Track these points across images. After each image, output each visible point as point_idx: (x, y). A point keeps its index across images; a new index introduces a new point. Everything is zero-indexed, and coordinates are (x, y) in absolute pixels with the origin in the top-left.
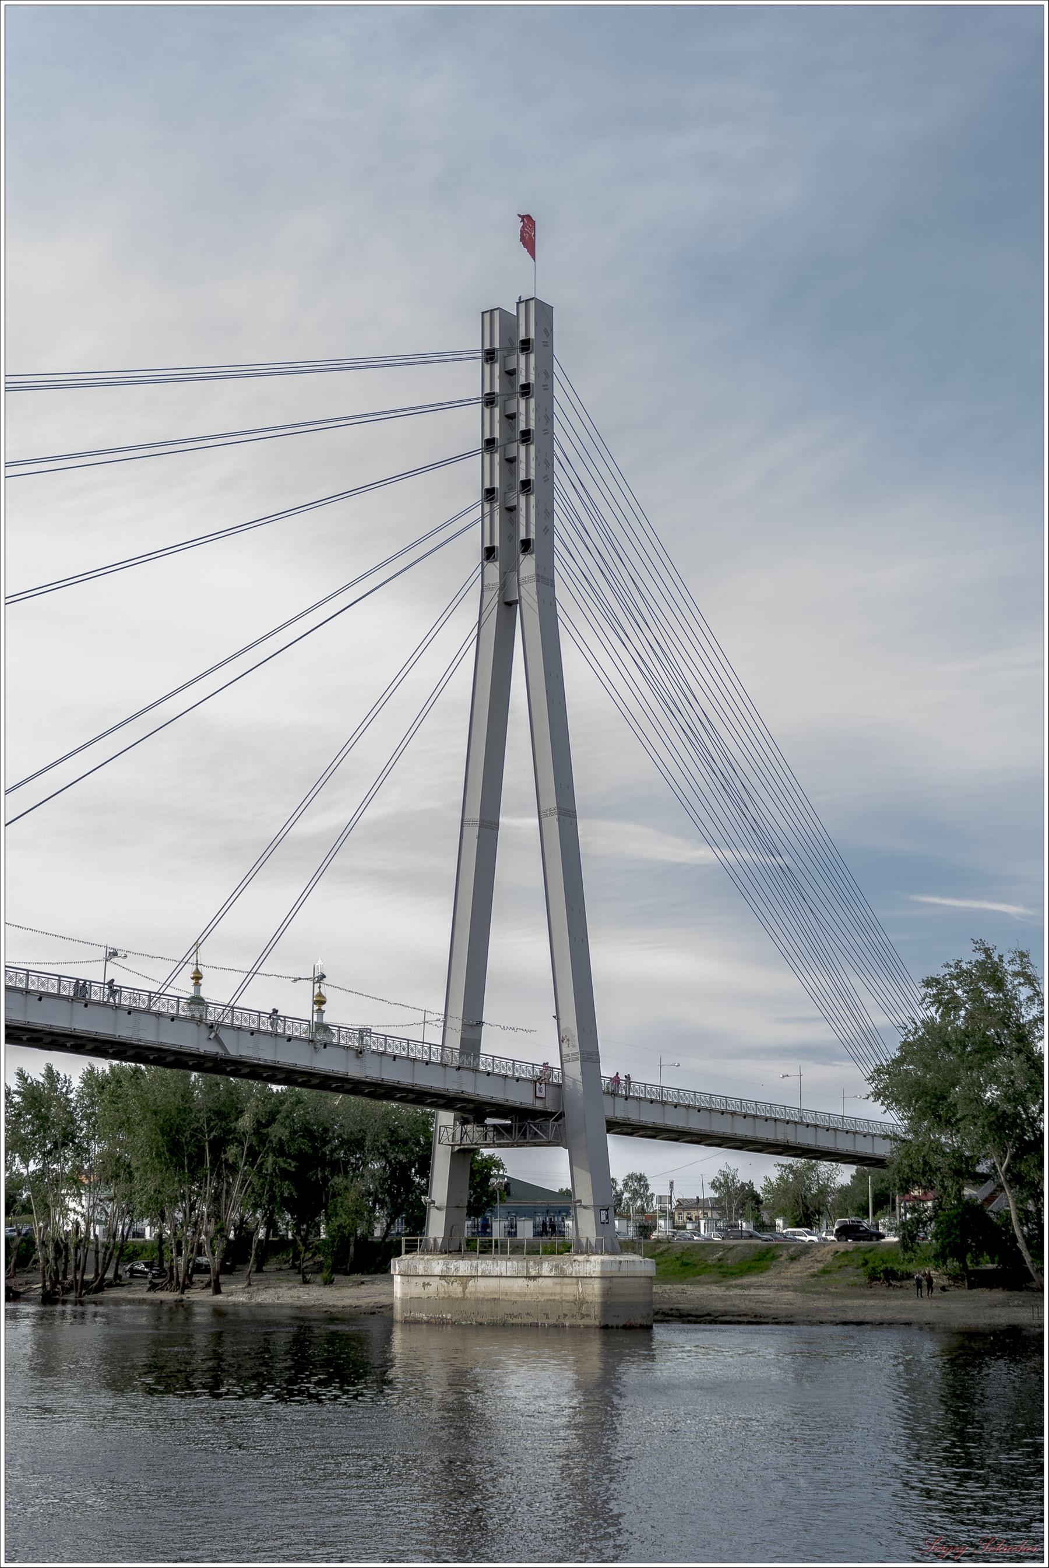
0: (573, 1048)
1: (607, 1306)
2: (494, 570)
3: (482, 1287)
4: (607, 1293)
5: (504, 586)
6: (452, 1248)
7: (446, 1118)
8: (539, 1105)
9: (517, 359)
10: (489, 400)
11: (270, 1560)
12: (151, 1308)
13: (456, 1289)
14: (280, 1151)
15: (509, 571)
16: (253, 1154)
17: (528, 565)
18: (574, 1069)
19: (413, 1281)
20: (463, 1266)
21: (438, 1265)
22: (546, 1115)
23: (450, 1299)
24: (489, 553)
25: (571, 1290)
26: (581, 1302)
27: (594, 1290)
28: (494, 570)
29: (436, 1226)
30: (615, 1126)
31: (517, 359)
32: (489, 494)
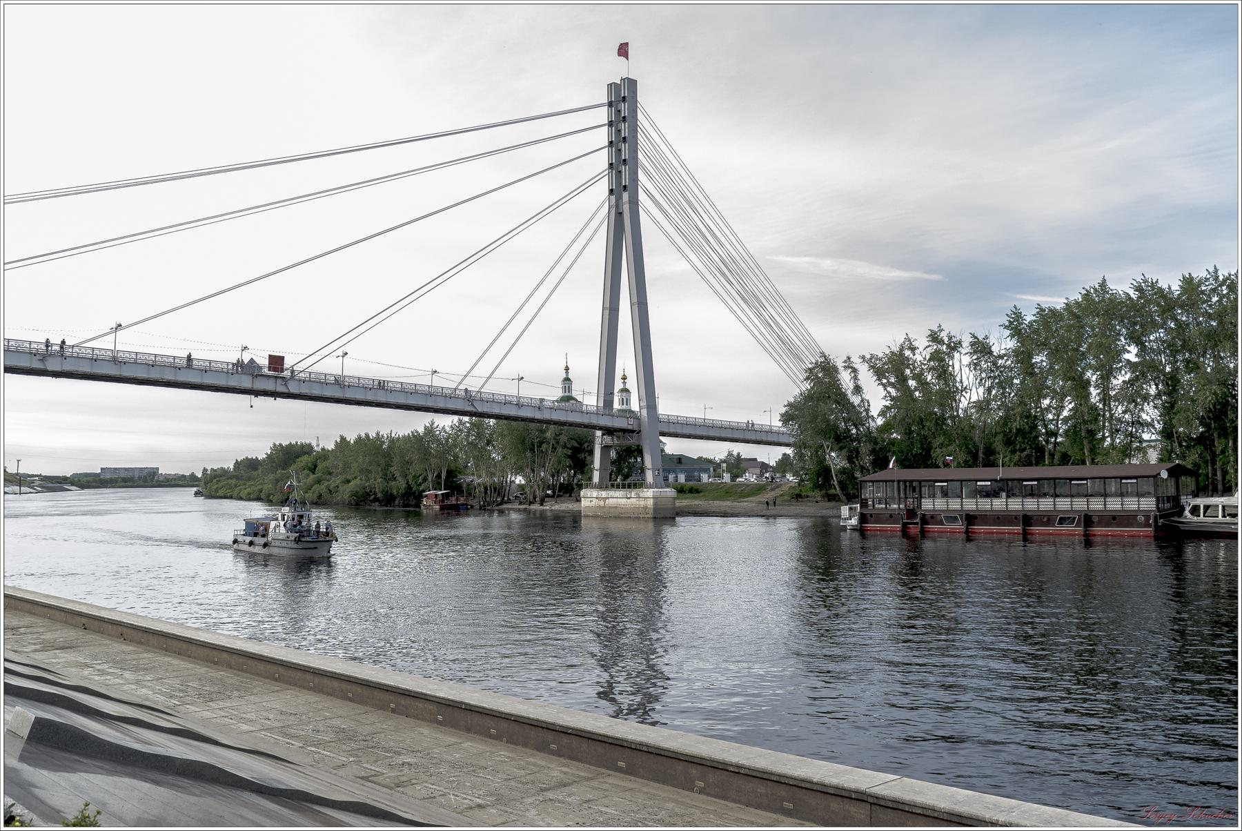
0: (644, 404)
1: (655, 510)
2: (613, 198)
3: (611, 502)
4: (655, 504)
5: (617, 206)
6: (601, 487)
7: (599, 433)
8: (630, 427)
9: (622, 102)
10: (610, 124)
11: (945, 757)
12: (521, 517)
13: (602, 503)
14: (565, 446)
15: (619, 199)
16: (554, 448)
17: (626, 196)
18: (644, 412)
19: (590, 499)
20: (604, 494)
21: (595, 493)
22: (632, 431)
23: (600, 507)
24: (611, 191)
25: (642, 503)
26: (646, 508)
27: (650, 503)
28: (613, 198)
29: (596, 477)
30: (663, 434)
31: (622, 102)
32: (611, 165)
